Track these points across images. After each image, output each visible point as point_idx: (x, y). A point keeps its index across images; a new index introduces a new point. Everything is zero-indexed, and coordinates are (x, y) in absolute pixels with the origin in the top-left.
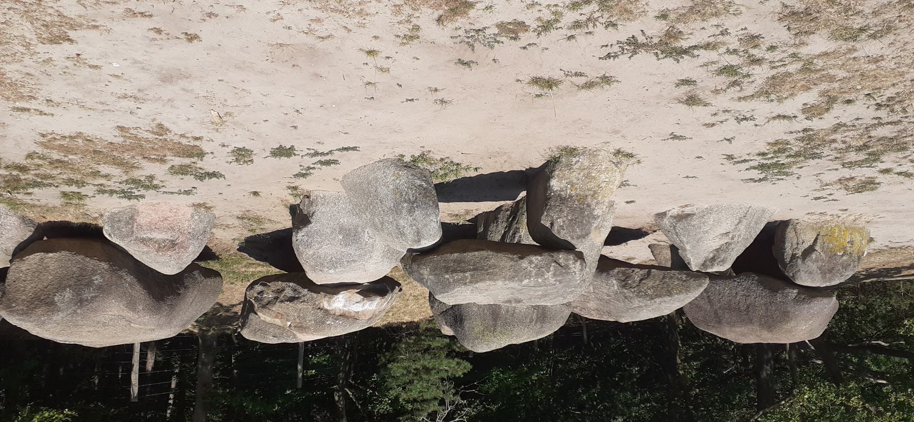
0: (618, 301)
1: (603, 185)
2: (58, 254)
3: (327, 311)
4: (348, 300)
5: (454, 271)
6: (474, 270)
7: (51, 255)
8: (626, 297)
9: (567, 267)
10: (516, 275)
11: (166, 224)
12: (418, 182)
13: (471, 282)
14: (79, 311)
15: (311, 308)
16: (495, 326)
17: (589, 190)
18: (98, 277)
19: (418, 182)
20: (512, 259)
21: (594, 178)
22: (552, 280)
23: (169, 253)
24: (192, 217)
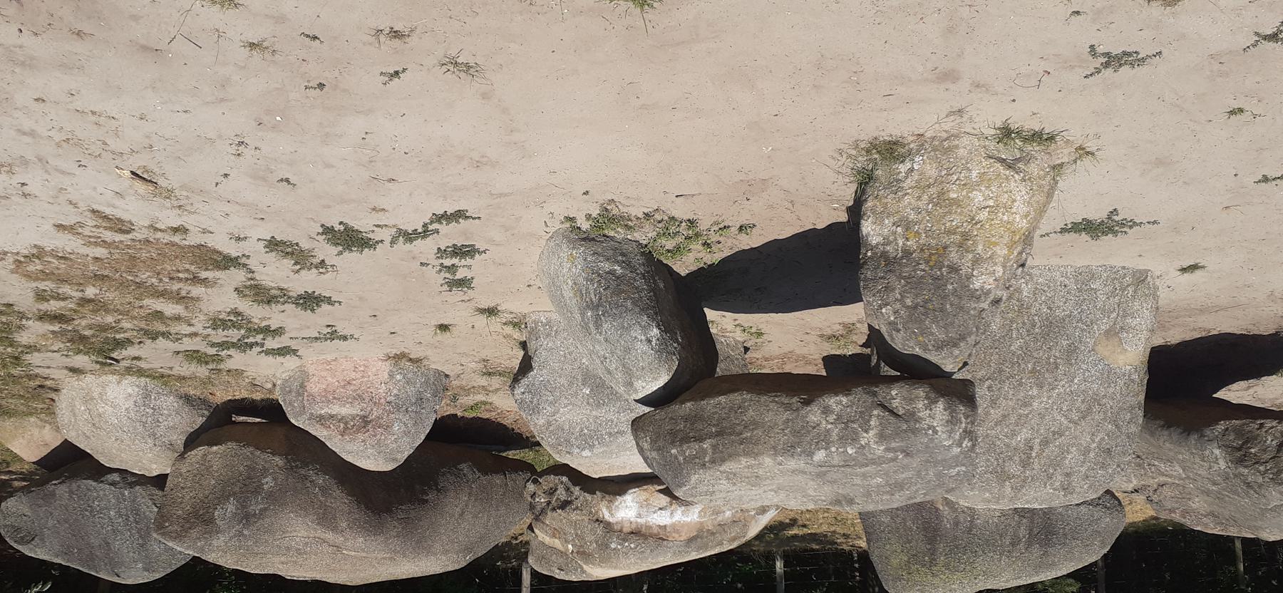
0: (1236, 493)
1: (983, 215)
2: (222, 447)
3: (608, 526)
4: (645, 505)
5: (686, 440)
6: (720, 434)
7: (215, 448)
8: (1248, 485)
9: (911, 416)
10: (800, 441)
11: (350, 391)
12: (606, 266)
13: (713, 462)
14: (246, 532)
15: (586, 519)
16: (933, 552)
17: (950, 232)
18: (269, 479)
19: (606, 266)
20: (788, 407)
21: (956, 202)
22: (879, 450)
23: (361, 436)
24: (391, 376)
